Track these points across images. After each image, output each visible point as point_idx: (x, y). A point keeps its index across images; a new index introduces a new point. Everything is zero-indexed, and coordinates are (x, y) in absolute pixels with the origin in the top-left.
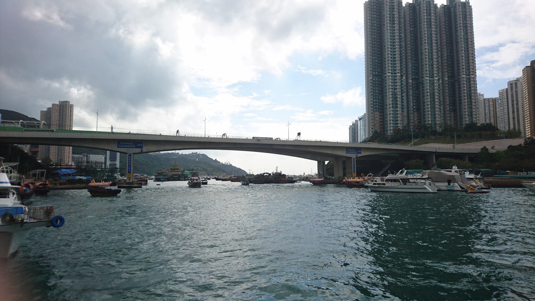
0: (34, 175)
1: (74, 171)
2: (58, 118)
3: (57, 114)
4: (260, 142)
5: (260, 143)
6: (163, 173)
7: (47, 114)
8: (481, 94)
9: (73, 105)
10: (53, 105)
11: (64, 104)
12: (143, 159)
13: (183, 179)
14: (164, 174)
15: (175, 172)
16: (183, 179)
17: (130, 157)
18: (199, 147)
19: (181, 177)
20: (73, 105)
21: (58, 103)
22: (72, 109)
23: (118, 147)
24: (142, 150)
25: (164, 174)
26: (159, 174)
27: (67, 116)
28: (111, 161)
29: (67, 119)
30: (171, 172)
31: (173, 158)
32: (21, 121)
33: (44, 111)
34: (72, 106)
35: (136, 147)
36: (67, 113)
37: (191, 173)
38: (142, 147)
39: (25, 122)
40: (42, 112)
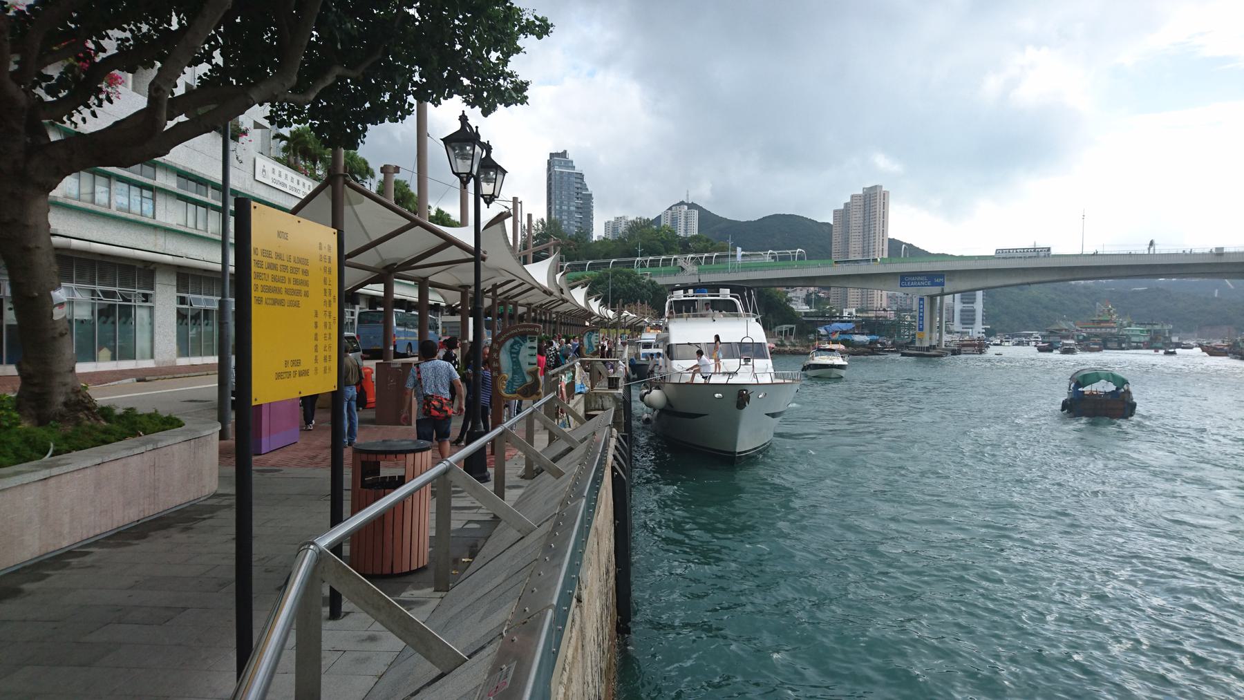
0: (781, 333)
1: (851, 325)
2: (862, 221)
3: (859, 214)
4: (1224, 260)
5: (1223, 261)
6: (1061, 330)
7: (843, 215)
8: (1053, 252)
9: (888, 192)
10: (852, 197)
11: (872, 193)
12: (1053, 296)
13: (1115, 345)
14: (1064, 332)
15: (1101, 328)
16: (1115, 345)
17: (921, 302)
18: (1085, 276)
19: (1111, 341)
20: (888, 192)
21: (861, 192)
22: (885, 229)
23: (901, 286)
24: (943, 290)
25: (1064, 332)
26: (1051, 332)
27: (878, 215)
28: (964, 303)
29: (877, 222)
30: (1086, 328)
31: (1135, 292)
32: (770, 251)
33: (840, 211)
34: (885, 195)
35: (934, 284)
36: (878, 210)
37: (1148, 331)
38: (942, 284)
39: (776, 252)
40: (835, 211)
